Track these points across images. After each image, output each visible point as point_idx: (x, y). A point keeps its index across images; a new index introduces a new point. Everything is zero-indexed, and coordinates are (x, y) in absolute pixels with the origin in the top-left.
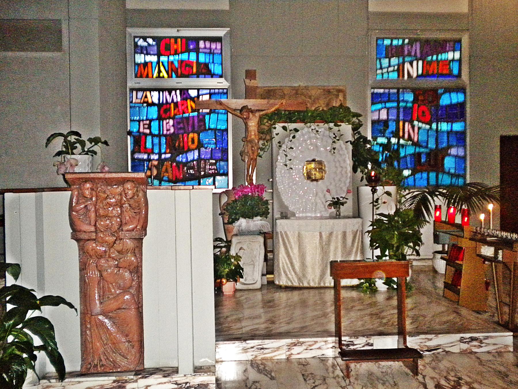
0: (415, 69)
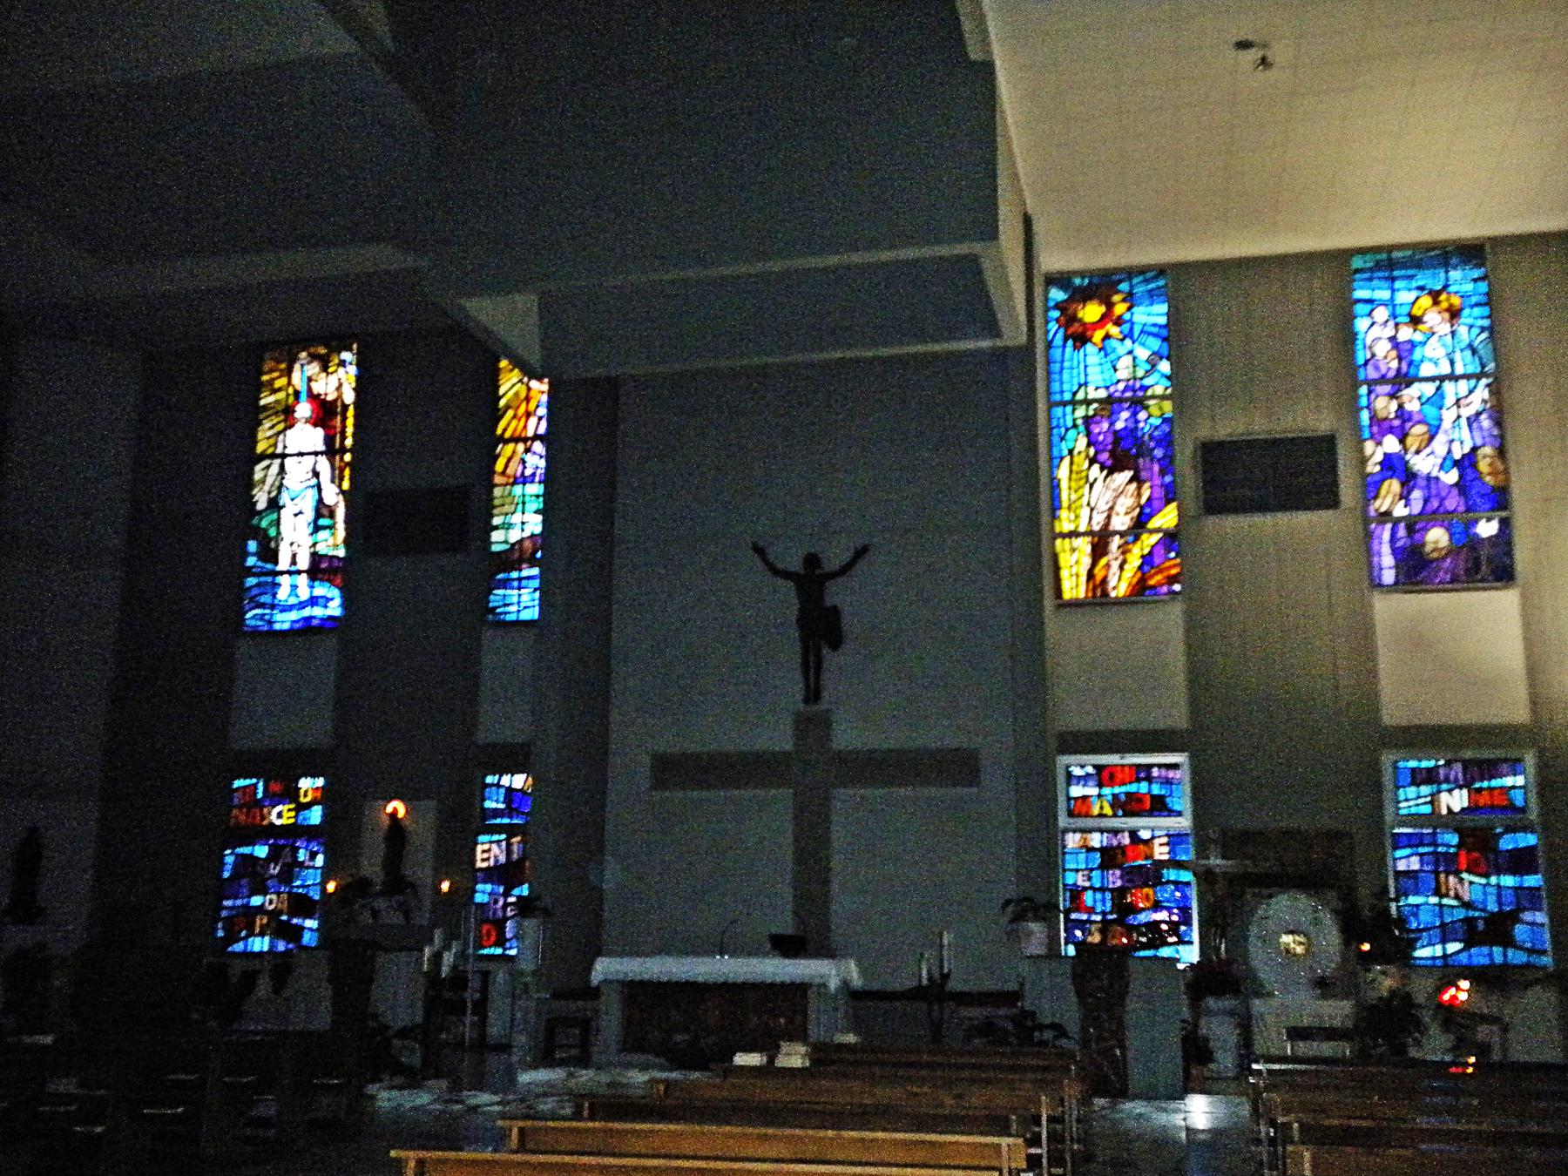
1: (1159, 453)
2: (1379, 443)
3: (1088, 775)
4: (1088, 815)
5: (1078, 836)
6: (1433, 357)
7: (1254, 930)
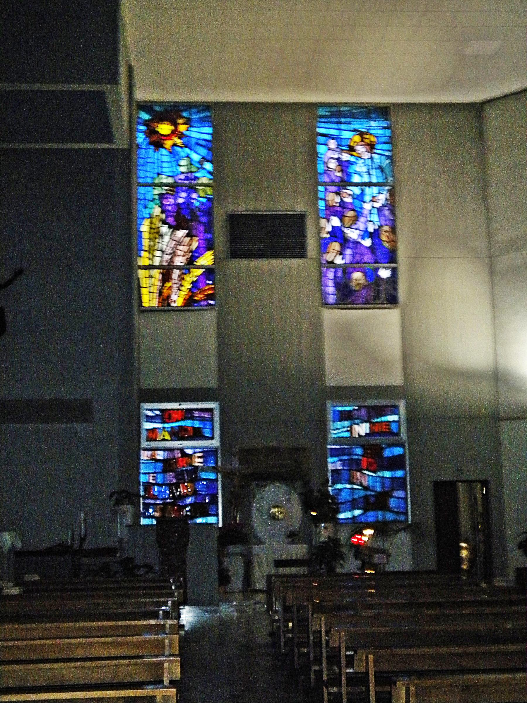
0: (363, 429)
1: (203, 219)
2: (328, 221)
3: (157, 415)
4: (155, 440)
5: (149, 453)
6: (360, 172)
7: (255, 506)
